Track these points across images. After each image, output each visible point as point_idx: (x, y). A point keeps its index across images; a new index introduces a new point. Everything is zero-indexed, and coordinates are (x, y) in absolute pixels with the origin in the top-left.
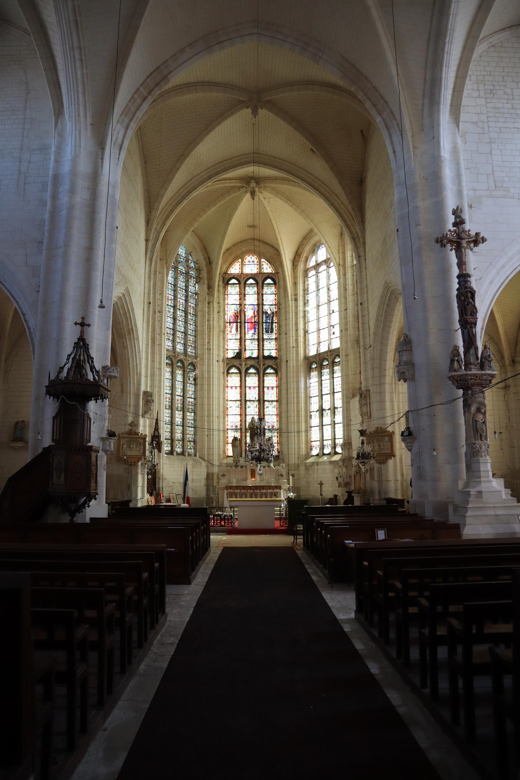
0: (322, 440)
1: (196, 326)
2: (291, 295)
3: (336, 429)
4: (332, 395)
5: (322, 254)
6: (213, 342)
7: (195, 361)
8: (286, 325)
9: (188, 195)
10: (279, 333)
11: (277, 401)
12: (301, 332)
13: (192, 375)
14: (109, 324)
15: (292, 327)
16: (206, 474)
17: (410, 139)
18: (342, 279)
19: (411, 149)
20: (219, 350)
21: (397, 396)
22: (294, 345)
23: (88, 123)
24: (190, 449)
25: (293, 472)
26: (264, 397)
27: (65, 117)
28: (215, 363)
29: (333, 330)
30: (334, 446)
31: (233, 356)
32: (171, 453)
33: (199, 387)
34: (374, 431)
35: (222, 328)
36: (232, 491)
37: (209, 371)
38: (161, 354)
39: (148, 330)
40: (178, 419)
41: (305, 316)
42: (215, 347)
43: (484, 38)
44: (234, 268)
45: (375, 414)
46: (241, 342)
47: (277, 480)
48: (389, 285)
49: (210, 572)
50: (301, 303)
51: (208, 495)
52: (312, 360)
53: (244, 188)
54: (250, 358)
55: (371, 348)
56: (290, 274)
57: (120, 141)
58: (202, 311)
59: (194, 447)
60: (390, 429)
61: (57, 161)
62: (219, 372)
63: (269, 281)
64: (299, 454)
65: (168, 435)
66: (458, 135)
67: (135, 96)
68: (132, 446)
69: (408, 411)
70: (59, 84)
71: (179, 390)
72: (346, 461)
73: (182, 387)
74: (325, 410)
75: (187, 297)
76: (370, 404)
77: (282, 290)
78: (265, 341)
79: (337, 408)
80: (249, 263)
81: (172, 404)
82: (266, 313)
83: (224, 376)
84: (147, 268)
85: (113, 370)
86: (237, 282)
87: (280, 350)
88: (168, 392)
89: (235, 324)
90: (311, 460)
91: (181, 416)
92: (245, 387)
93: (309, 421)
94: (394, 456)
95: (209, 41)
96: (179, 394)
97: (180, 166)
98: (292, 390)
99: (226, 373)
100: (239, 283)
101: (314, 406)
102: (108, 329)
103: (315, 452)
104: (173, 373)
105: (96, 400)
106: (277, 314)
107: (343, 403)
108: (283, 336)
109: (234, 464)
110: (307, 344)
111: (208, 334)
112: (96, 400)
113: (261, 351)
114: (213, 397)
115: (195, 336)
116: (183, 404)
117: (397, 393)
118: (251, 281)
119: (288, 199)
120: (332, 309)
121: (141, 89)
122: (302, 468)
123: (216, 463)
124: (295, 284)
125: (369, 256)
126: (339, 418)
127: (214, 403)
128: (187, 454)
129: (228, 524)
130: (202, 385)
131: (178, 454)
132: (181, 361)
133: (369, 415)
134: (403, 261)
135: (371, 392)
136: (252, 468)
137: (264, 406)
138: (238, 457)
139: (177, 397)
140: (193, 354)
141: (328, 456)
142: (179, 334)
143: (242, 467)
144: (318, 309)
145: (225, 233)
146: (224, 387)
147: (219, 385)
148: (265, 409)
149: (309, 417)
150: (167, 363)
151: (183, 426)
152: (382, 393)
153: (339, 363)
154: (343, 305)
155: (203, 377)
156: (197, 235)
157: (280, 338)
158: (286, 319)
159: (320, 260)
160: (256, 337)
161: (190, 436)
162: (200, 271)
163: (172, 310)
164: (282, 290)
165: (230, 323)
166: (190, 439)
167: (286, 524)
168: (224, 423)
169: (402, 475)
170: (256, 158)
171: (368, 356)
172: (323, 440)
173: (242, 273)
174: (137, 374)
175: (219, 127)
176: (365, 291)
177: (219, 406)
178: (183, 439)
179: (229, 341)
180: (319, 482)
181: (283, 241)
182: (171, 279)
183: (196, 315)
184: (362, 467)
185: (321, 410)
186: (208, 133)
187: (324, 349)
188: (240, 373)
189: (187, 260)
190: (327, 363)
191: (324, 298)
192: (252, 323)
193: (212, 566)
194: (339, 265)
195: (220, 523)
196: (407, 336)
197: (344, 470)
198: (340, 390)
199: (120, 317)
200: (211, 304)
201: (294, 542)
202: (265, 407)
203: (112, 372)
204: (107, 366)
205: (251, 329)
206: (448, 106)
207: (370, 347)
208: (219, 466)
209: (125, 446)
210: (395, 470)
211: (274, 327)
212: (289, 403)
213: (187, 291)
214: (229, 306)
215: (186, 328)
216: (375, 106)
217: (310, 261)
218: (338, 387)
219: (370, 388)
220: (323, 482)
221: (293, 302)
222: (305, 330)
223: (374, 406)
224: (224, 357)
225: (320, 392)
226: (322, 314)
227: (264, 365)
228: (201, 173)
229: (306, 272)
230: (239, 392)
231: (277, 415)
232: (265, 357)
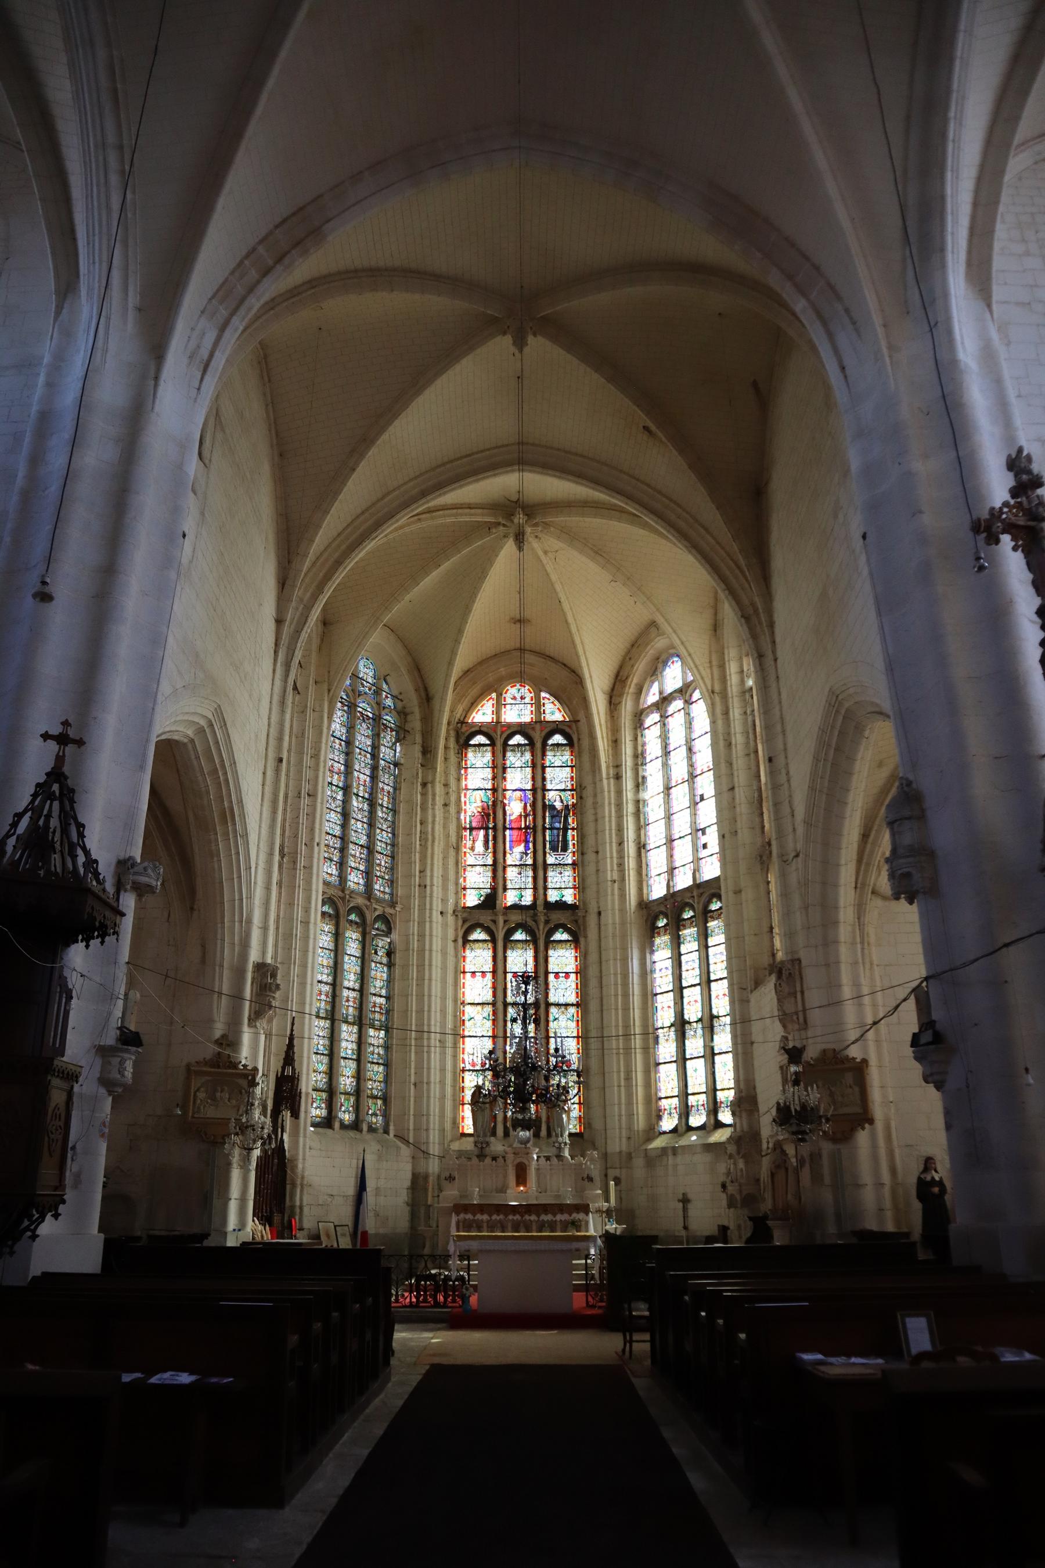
0: (684, 1094)
1: (394, 835)
2: (608, 767)
3: (717, 1066)
4: (704, 986)
5: (673, 676)
6: (432, 870)
7: (391, 911)
8: (596, 833)
9: (376, 530)
10: (581, 852)
11: (577, 1005)
12: (631, 849)
13: (382, 943)
14: (144, 755)
15: (611, 837)
16: (409, 1176)
17: (880, 331)
18: (720, 722)
19: (885, 351)
20: (445, 888)
21: (867, 971)
22: (616, 877)
23: (131, 305)
24: (375, 1114)
25: (616, 1172)
27: (80, 297)
28: (436, 915)
29: (703, 839)
30: (714, 1108)
31: (476, 903)
32: (327, 1122)
33: (397, 971)
34: (817, 1060)
35: (453, 839)
36: (469, 1216)
37: (422, 936)
38: (310, 890)
39: (273, 820)
40: (347, 1045)
41: (638, 813)
42: (437, 881)
43: (1023, 144)
44: (480, 712)
45: (815, 1016)
46: (494, 872)
47: (580, 1191)
48: (840, 697)
49: (366, 1452)
50: (628, 784)
51: (413, 1227)
52: (657, 909)
53: (501, 528)
54: (515, 907)
55: (800, 859)
56: (603, 722)
57: (204, 353)
58: (410, 802)
59: (384, 1112)
60: (855, 1052)
61: (50, 385)
62: (444, 938)
63: (558, 739)
64: (630, 1128)
65: (321, 1080)
66: (990, 323)
67: (246, 262)
68: (218, 1094)
69: (926, 979)
70: (72, 231)
71: (352, 977)
72: (746, 1141)
73: (358, 969)
74: (689, 1023)
75: (374, 768)
76: (802, 992)
77: (586, 758)
78: (550, 869)
79: (718, 1017)
80: (513, 702)
81: (333, 1007)
82: (553, 807)
83: (456, 949)
84: (278, 683)
85: (145, 869)
86: (488, 742)
87: (584, 888)
88: (325, 978)
89: (482, 833)
90: (658, 1143)
91: (354, 1037)
92: (505, 973)
94: (871, 1121)
95: (416, 158)
96: (351, 985)
97: (357, 464)
98: (612, 978)
99: (460, 941)
100: (493, 744)
101: (665, 1016)
102: (142, 768)
103: (668, 1124)
104: (338, 937)
105: (87, 940)
106: (576, 809)
107: (732, 1003)
108: (590, 857)
109: (476, 1152)
110: (644, 873)
111: (421, 853)
112: (87, 940)
113: (541, 891)
115: (393, 857)
116: (361, 1008)
117: (868, 966)
118: (518, 739)
119: (597, 551)
120: (699, 792)
121: (261, 249)
122: (639, 1162)
123: (435, 1149)
124: (615, 743)
125: (784, 651)
126: (723, 1040)
127: (433, 1009)
128: (365, 1127)
129: (454, 1301)
130: (406, 966)
131: (343, 1126)
132: (358, 910)
133: (801, 1019)
134: (887, 603)
135: (804, 963)
136: (518, 1160)
138: (485, 1135)
139: (346, 993)
140: (387, 896)
141: (699, 1133)
142: (353, 850)
143: (494, 1159)
144: (668, 795)
145: (460, 632)
146: (456, 972)
147: (444, 968)
149: (651, 1041)
150: (324, 914)
151: (358, 1060)
152: (830, 965)
153: (718, 914)
154: (724, 780)
155: (407, 950)
156: (401, 639)
157: (583, 862)
158: (596, 820)
159: (669, 689)
160: (530, 861)
161: (374, 1085)
162: (406, 714)
163: (340, 796)
164: (586, 758)
165: (471, 829)
166: (375, 1092)
167: (601, 1301)
168: (455, 1056)
169: (893, 1171)
170: (523, 455)
171: (793, 879)
172: (687, 1095)
173: (498, 722)
174: (241, 921)
175: (444, 378)
176: (779, 728)
177: (445, 1017)
178: (358, 1092)
179: (469, 868)
180: (681, 1197)
181: (587, 647)
182: (338, 725)
183: (394, 811)
184: (790, 1150)
185: (681, 1025)
186: (419, 392)
187: (683, 881)
188: (493, 940)
189: (378, 692)
190: (691, 913)
191: (679, 769)
192: (520, 829)
193: (379, 1430)
194: (713, 692)
195: (435, 1298)
196: (909, 783)
197: (741, 1164)
198: (725, 975)
199: (200, 778)
200: (429, 785)
201: (624, 1350)
202: (551, 1018)
203: (140, 874)
204: (131, 858)
205: (519, 842)
206: (962, 268)
207: (797, 856)
208: (441, 1158)
209: (201, 1095)
210: (875, 1158)
211: (570, 838)
212: (605, 1007)
213: (375, 756)
214: (468, 792)
215: (371, 836)
216: (790, 277)
217: (647, 694)
218: (719, 967)
219: (802, 954)
220: (690, 1196)
221: (612, 781)
222: (639, 843)
223: (814, 998)
224: (457, 903)
225: (677, 982)
226: (679, 814)
227: (547, 922)
228: (405, 484)
229: (638, 724)
230: (490, 985)
231: (578, 1037)
232: (548, 905)
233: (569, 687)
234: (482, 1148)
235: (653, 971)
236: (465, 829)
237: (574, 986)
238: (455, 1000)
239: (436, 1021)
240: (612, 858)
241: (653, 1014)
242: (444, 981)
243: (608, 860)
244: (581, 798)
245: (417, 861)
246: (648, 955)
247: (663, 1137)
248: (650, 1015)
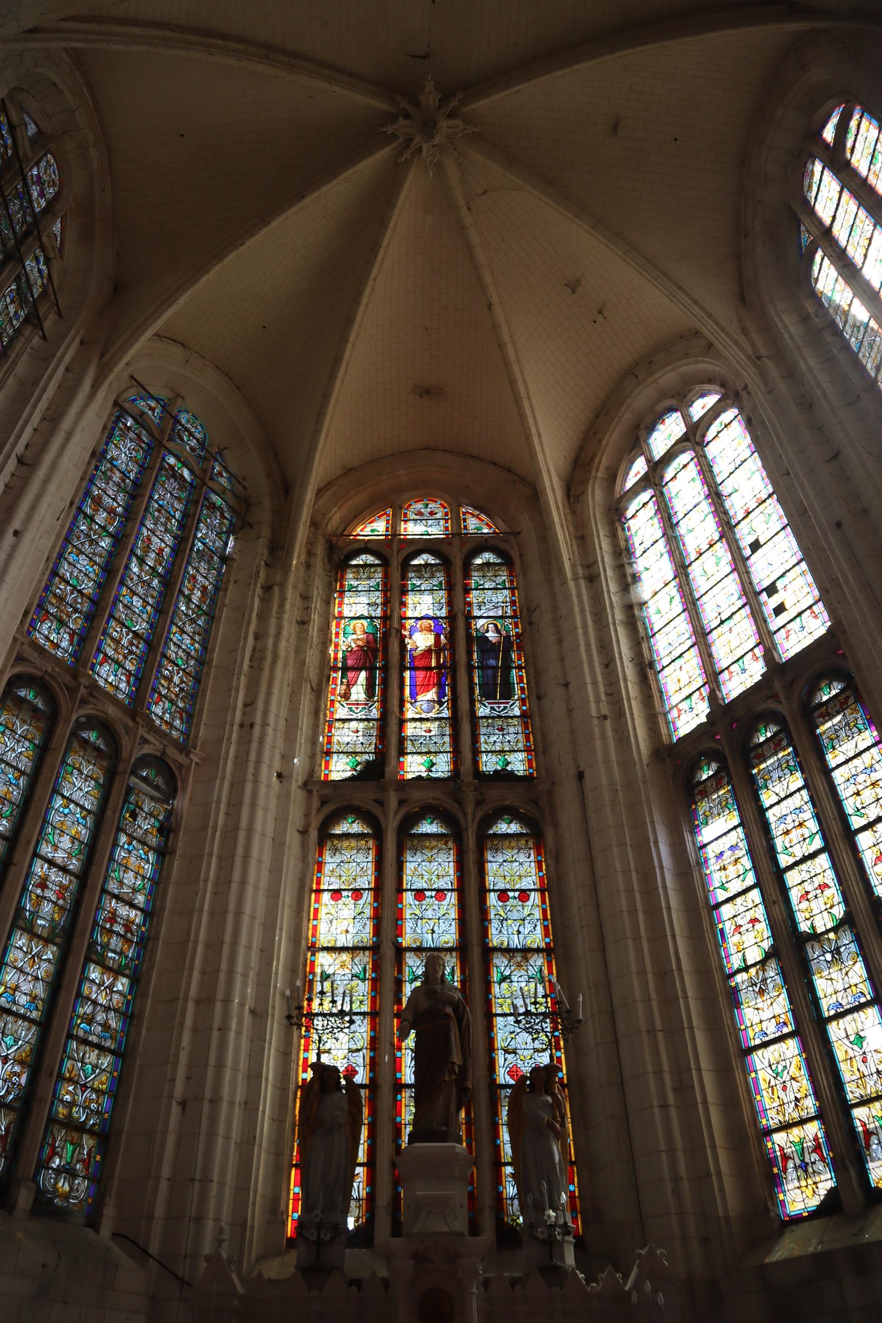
2: (573, 566)
6: (267, 702)
7: (181, 758)
10: (536, 694)
11: (547, 951)
12: (628, 670)
22: (605, 710)
24: (68, 1171)
26: (484, 932)
37: (234, 806)
74: (815, 937)
77: (536, 573)
83: (304, 846)
89: (363, 675)
92: (400, 890)
93: (726, 1020)
96: (60, 856)
99: (314, 835)
101: (746, 937)
103: (801, 1196)
108: (555, 693)
114: (239, 913)
124: (583, 539)
130: (196, 859)
132: (105, 726)
137: (487, 972)
148: (496, 989)
149: (722, 1000)
179: (338, 724)
188: (378, 835)
200: (276, 589)
202: (495, 976)
221: (582, 582)
224: (312, 772)
225: (765, 863)
229: (616, 514)
233: (505, 486)
234: (319, 1243)
235: (702, 863)
236: (335, 669)
237: (537, 914)
238: (297, 936)
239: (247, 968)
240: (595, 683)
241: (717, 947)
242: (273, 896)
243: (590, 687)
244: (531, 623)
245: (242, 686)
246: (687, 837)
247: (799, 1231)
248: (710, 947)
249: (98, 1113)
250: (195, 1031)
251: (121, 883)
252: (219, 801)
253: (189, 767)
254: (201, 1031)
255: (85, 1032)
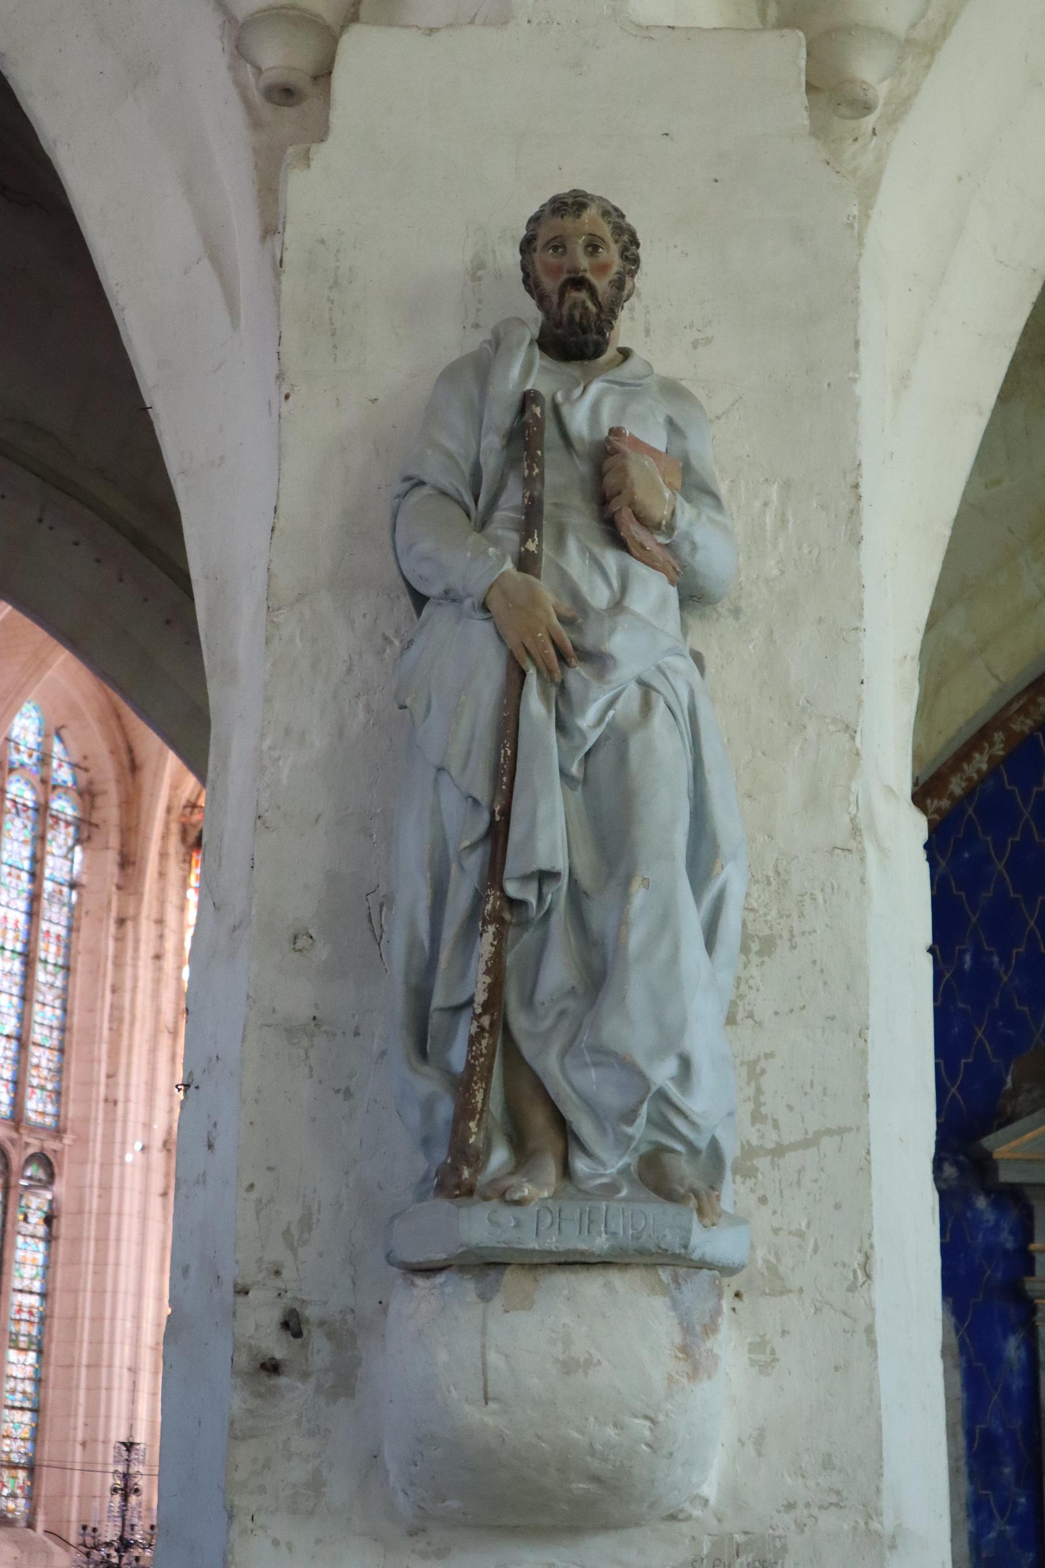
24: (13, 1496)
130: (77, 1241)
200: (129, 925)
249: (26, 1454)
250: (88, 1389)
251: (22, 1277)
252: (91, 1186)
253: (62, 1152)
254: (93, 1389)
255: (12, 1401)
